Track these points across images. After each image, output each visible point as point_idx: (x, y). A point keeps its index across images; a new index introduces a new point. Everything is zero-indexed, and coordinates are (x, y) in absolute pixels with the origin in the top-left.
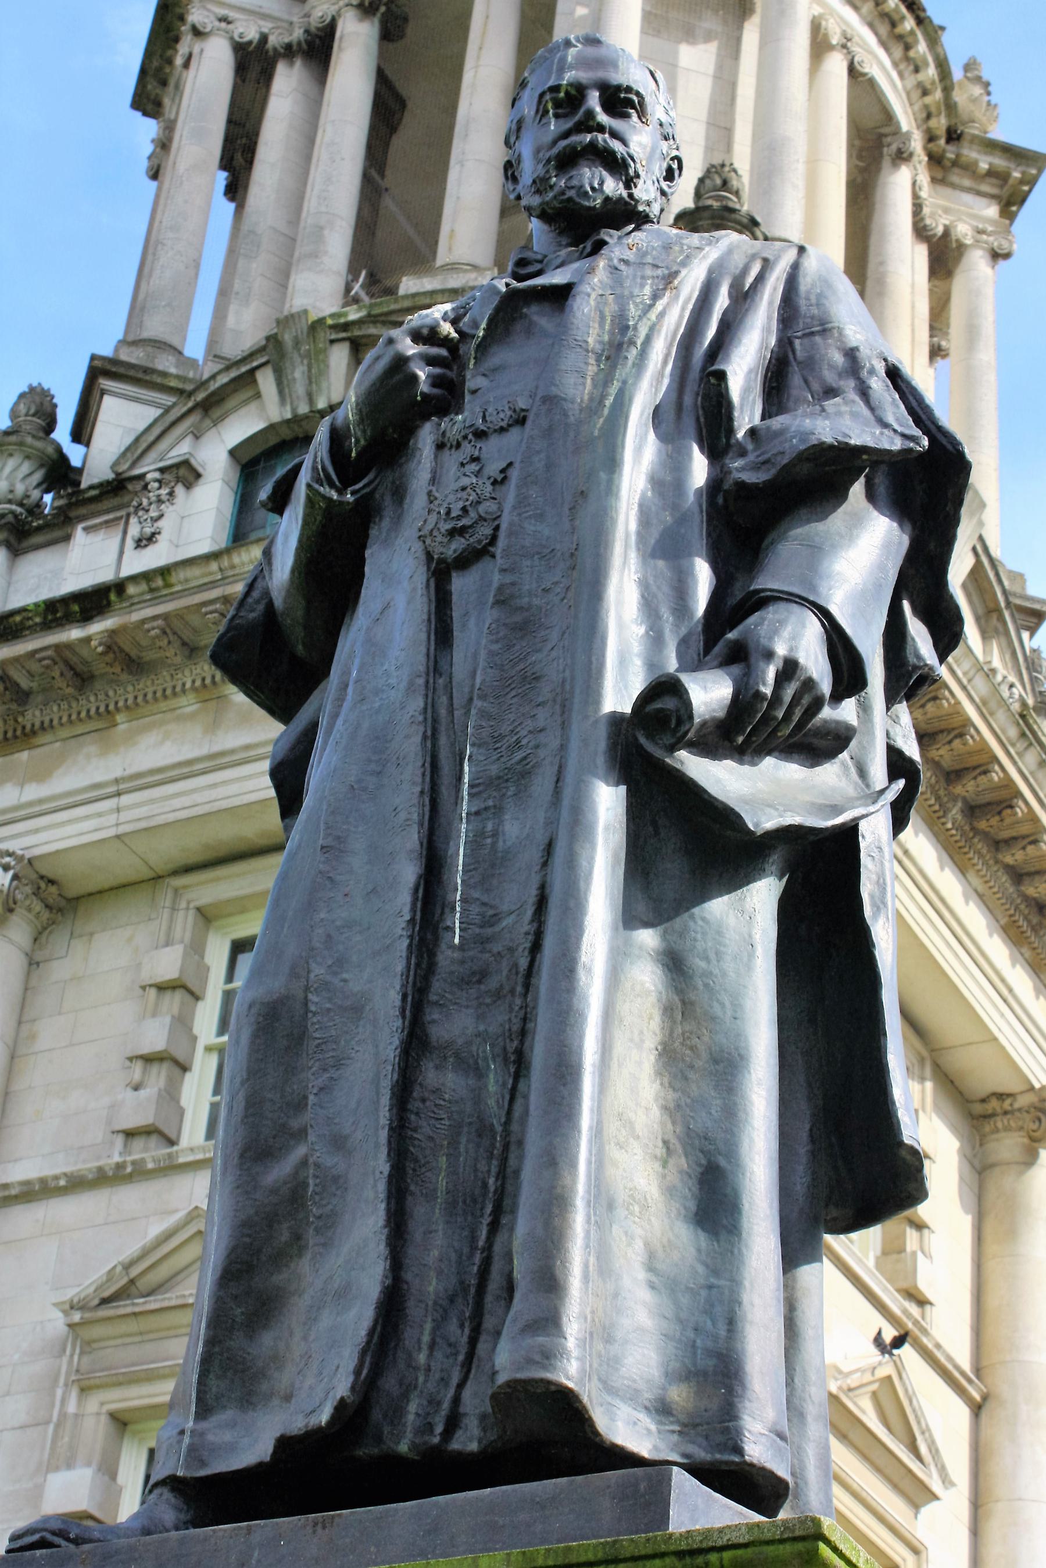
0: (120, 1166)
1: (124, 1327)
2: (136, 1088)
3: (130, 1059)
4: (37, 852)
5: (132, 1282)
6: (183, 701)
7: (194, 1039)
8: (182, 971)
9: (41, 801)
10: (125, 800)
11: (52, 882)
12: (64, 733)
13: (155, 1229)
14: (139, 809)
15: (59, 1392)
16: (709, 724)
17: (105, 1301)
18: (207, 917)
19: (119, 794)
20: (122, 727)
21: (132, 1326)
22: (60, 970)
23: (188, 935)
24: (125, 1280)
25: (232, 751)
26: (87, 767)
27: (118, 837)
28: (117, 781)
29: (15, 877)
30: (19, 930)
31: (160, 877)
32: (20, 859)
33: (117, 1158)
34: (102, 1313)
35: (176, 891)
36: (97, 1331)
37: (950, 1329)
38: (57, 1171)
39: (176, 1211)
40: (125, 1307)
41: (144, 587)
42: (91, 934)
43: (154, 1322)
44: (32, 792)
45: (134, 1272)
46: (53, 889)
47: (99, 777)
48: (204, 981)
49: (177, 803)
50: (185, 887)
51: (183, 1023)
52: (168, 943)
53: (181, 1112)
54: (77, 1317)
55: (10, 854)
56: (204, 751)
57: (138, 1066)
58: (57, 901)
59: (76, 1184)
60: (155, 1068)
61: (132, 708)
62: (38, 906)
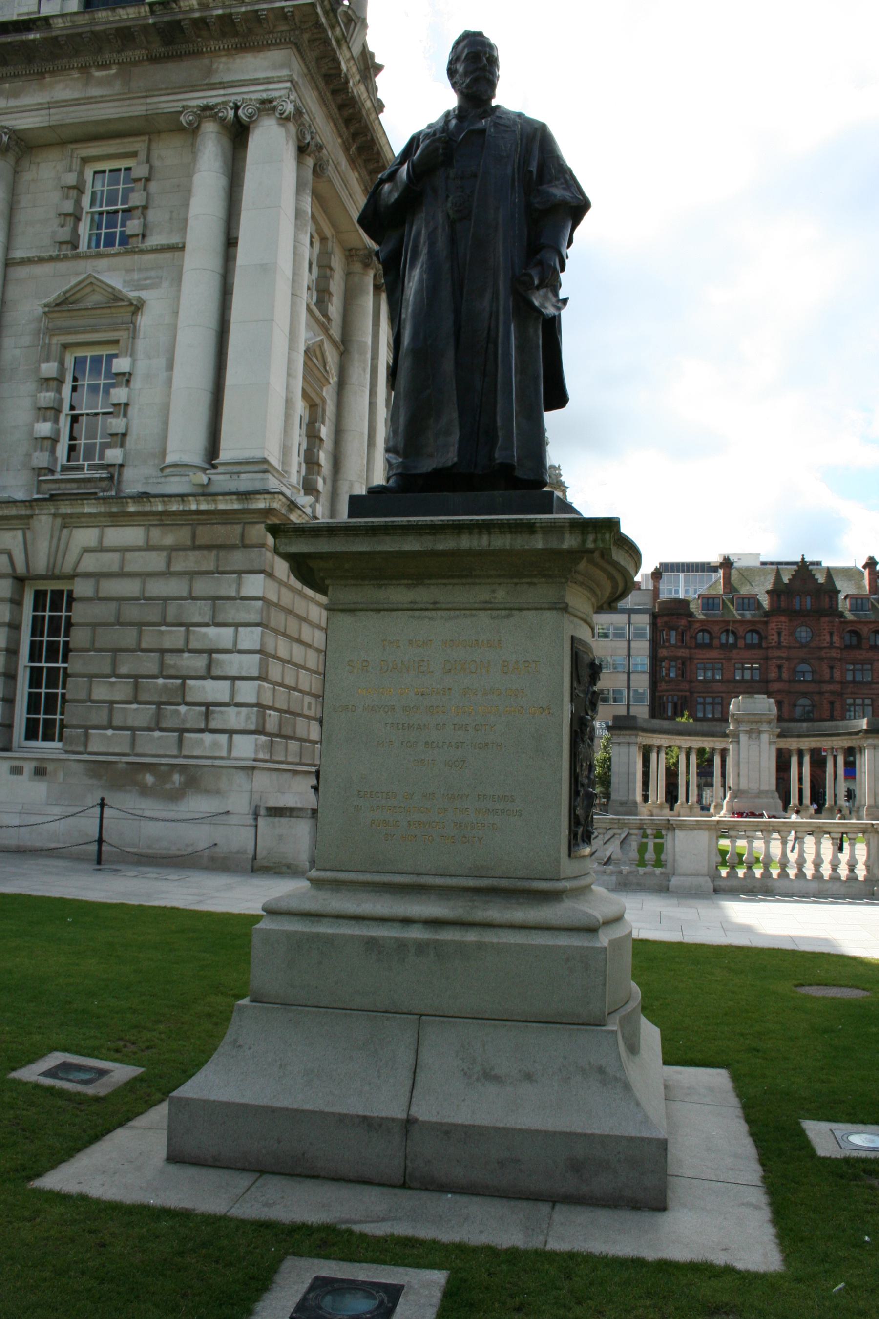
0: (58, 255)
1: (65, 314)
2: (62, 226)
3: (59, 215)
4: (18, 127)
5: (67, 298)
6: (73, 72)
7: (82, 209)
8: (77, 182)
9: (17, 107)
10: (52, 111)
11: (22, 140)
12: (23, 79)
13: (74, 282)
14: (58, 116)
15: (41, 336)
16: (452, 113)
17: (57, 305)
18: (85, 161)
19: (49, 108)
20: (48, 79)
21: (68, 314)
22: (27, 176)
23: (78, 168)
24: (64, 298)
25: (96, 97)
26: (33, 97)
27: (50, 126)
28: (48, 103)
29: (9, 138)
30: (11, 158)
31: (65, 143)
32: (10, 130)
33: (57, 253)
34: (56, 309)
35: (72, 149)
36: (55, 315)
37: (336, 332)
38: (34, 255)
39: (81, 274)
40: (65, 308)
41: (161, 7)
42: (39, 163)
43: (75, 313)
44: (12, 103)
45: (68, 295)
46: (23, 143)
47: (40, 101)
48: (84, 186)
49: (73, 115)
50: (76, 149)
51: (78, 203)
52: (70, 171)
53: (79, 236)
54: (47, 309)
55: (7, 128)
56: (83, 95)
57: (62, 217)
58: (23, 147)
59: (41, 260)
60: (68, 219)
61: (52, 73)
62: (17, 149)
